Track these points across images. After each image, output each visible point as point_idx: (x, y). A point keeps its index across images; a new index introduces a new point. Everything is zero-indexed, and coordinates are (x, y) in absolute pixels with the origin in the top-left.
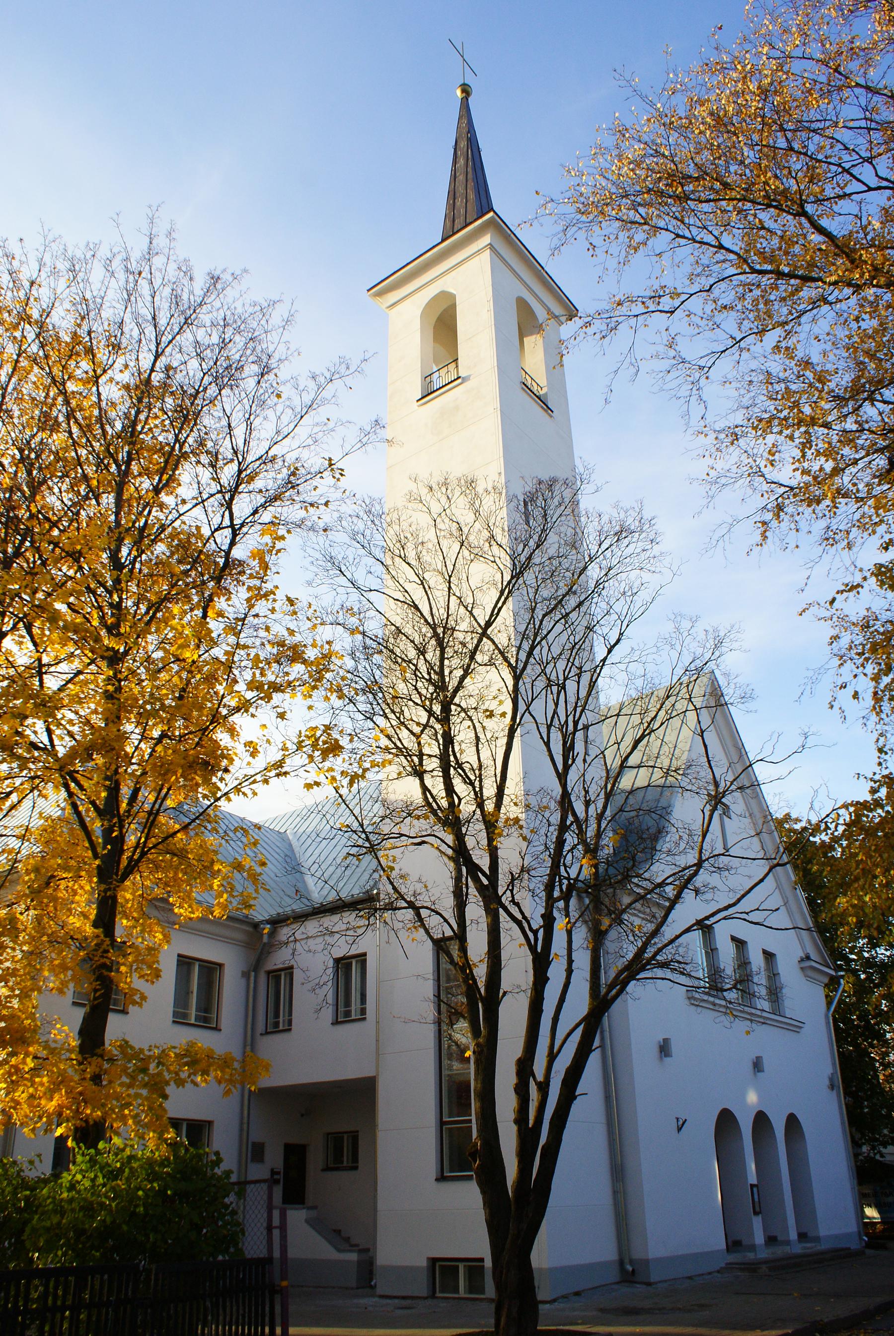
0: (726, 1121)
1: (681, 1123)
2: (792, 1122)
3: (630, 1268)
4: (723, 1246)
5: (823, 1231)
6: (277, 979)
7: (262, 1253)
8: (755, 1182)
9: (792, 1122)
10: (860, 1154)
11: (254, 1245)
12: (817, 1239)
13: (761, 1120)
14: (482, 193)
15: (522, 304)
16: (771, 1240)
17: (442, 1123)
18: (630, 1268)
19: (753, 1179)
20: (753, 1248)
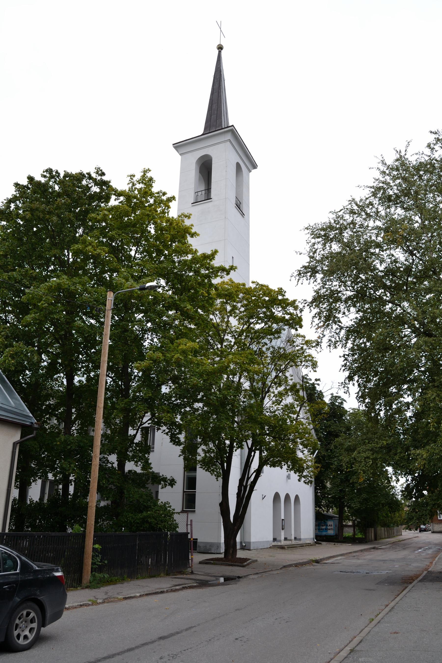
0: (277, 496)
1: (264, 496)
2: (297, 497)
3: (244, 544)
4: (272, 540)
5: (302, 537)
6: (147, 433)
7: (185, 531)
8: (283, 518)
9: (297, 497)
10: (438, 507)
11: (181, 529)
12: (300, 539)
13: (287, 497)
14: (214, 117)
15: (238, 165)
16: (286, 539)
17: (184, 492)
18: (244, 544)
19: (283, 517)
20: (280, 541)
